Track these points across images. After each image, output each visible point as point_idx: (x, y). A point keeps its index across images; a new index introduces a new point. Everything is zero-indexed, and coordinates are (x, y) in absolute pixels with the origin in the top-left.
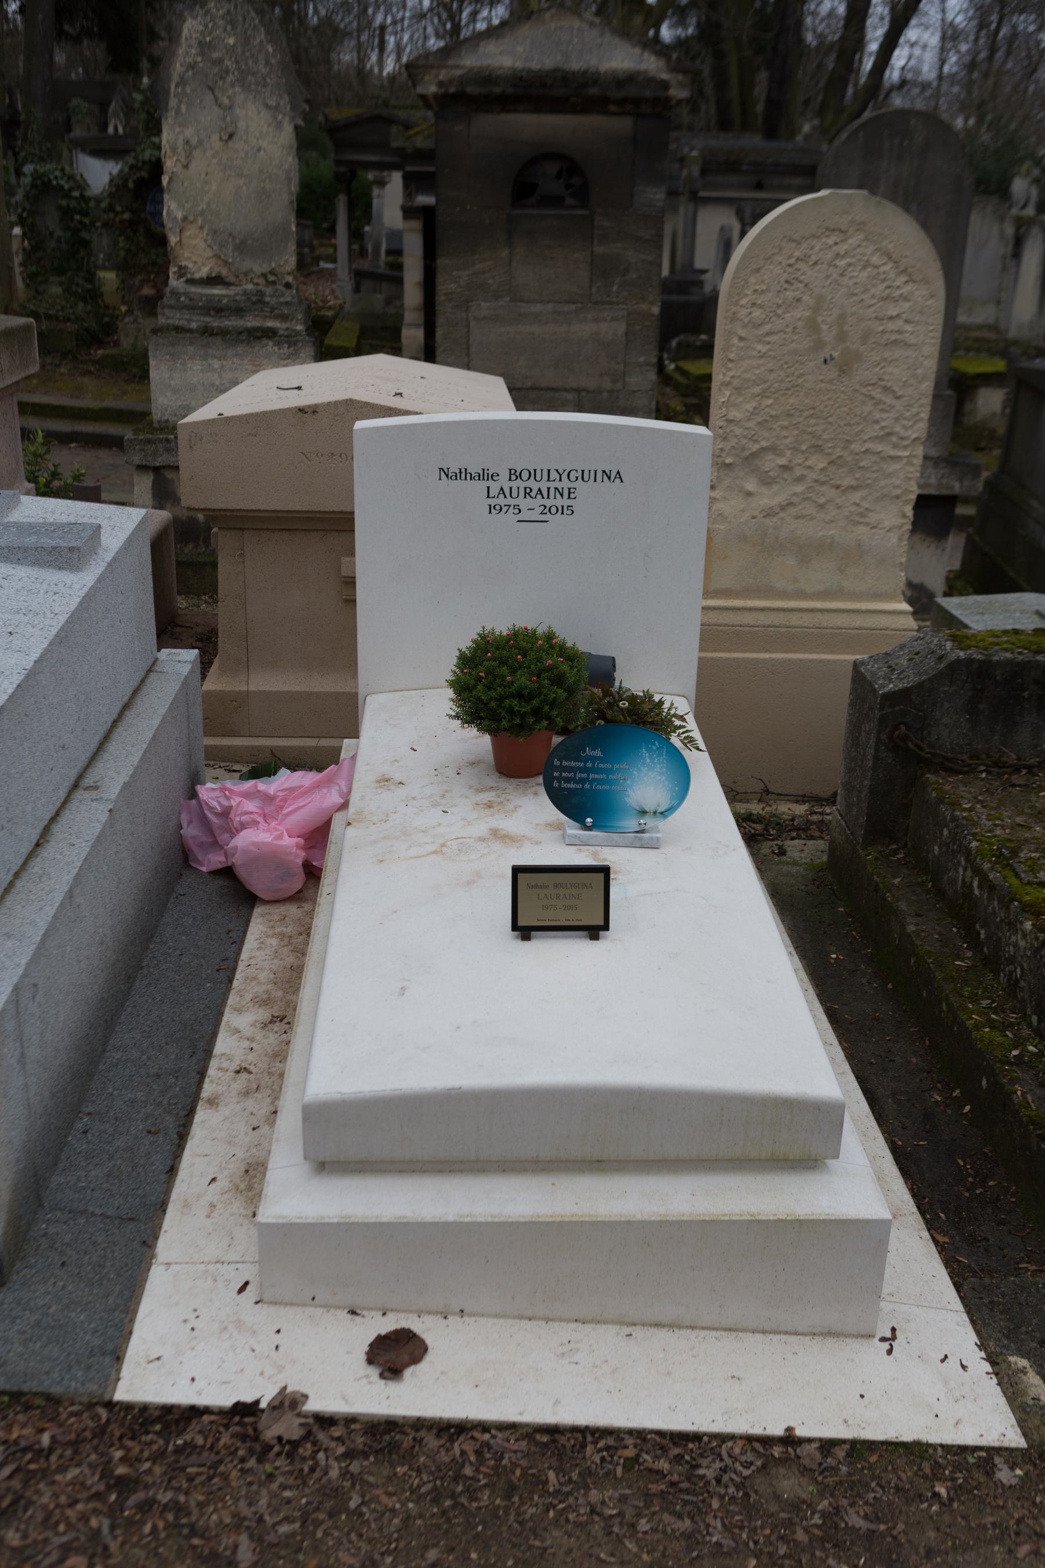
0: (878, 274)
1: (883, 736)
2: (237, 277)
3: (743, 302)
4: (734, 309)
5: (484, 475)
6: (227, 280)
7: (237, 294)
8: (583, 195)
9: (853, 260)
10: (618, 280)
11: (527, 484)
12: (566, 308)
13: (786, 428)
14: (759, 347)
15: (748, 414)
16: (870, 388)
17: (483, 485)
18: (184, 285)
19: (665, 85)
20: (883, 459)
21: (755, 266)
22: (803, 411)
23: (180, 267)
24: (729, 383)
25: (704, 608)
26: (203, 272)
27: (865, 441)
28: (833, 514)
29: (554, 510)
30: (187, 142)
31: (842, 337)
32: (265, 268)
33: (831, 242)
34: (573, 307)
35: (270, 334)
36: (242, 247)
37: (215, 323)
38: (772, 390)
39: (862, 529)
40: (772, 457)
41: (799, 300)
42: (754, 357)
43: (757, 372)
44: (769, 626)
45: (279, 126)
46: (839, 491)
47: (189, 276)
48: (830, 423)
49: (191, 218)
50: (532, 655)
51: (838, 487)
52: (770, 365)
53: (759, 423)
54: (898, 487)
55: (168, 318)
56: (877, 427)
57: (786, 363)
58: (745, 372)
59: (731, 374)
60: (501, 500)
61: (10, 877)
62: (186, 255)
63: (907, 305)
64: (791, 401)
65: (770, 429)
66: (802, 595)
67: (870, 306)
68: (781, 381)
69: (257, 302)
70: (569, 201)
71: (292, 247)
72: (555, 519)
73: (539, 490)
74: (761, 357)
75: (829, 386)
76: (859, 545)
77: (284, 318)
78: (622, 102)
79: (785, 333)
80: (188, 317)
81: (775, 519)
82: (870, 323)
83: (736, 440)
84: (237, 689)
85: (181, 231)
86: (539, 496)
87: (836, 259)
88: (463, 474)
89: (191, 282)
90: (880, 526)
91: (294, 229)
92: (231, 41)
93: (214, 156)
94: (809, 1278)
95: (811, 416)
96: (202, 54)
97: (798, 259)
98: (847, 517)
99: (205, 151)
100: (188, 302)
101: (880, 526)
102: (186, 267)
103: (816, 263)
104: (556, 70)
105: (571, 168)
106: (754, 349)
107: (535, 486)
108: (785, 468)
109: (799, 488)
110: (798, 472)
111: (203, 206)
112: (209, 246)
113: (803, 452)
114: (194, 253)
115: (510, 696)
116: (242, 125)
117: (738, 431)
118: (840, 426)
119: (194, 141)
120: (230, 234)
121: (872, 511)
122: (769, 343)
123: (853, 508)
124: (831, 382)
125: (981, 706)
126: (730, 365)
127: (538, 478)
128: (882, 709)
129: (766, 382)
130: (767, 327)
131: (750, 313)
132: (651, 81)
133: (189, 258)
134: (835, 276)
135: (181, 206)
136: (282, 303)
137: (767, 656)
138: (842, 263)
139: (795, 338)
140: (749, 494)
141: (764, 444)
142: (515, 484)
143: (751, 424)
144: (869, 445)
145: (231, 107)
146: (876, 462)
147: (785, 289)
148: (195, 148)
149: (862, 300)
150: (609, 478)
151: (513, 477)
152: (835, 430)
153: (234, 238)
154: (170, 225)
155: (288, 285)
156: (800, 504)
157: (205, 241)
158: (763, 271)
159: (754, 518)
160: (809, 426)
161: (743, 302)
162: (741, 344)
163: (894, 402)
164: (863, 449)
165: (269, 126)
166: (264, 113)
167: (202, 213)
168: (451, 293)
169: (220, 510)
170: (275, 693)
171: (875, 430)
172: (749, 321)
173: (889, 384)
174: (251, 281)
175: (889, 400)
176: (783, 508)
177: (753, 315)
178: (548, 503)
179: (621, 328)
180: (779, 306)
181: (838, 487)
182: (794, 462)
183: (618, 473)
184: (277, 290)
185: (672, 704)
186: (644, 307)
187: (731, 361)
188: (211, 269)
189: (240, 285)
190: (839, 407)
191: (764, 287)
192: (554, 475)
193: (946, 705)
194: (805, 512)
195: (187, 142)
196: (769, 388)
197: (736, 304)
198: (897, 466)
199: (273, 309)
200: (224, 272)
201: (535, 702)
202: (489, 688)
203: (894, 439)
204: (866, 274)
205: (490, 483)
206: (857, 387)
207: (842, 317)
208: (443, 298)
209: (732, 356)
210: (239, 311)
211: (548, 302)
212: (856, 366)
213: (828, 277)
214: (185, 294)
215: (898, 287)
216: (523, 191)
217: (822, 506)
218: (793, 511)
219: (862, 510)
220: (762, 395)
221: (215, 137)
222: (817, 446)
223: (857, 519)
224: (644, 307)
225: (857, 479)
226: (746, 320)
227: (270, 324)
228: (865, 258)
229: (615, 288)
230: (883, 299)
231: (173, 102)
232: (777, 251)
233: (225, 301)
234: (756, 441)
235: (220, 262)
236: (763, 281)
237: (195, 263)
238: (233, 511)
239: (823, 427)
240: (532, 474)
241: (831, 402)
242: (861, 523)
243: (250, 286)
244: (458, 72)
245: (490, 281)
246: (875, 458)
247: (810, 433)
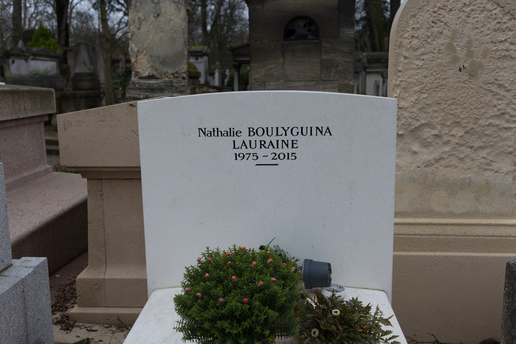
0: (491, 15)
2: (161, 75)
3: (406, 35)
4: (400, 40)
6: (157, 77)
7: (161, 83)
8: (316, 34)
9: (474, 8)
10: (334, 70)
11: (262, 138)
13: (437, 111)
14: (417, 62)
15: (412, 103)
16: (490, 85)
17: (231, 139)
18: (138, 80)
20: (500, 129)
21: (412, 14)
22: (447, 101)
23: (136, 72)
24: (399, 85)
25: (396, 224)
26: (146, 74)
27: (488, 118)
28: (469, 164)
29: (282, 156)
30: (139, 19)
31: (470, 54)
32: (173, 71)
34: (313, 83)
36: (163, 62)
38: (427, 88)
39: (488, 174)
40: (428, 130)
41: (441, 33)
42: (415, 69)
43: (417, 78)
44: (432, 235)
46: (472, 149)
47: (140, 76)
48: (465, 108)
49: (141, 51)
50: (246, 275)
51: (471, 148)
52: (424, 73)
53: (419, 109)
54: (511, 146)
55: (130, 94)
56: (495, 109)
57: (435, 71)
58: (409, 78)
59: (400, 79)
60: (244, 150)
62: (139, 67)
63: (511, 33)
64: (439, 95)
65: (426, 112)
66: (452, 215)
67: (487, 35)
68: (432, 83)
70: (310, 37)
72: (283, 163)
73: (271, 142)
74: (419, 68)
75: (463, 85)
76: (488, 183)
79: (433, 53)
80: (138, 93)
81: (432, 168)
82: (487, 45)
83: (405, 120)
84: (98, 277)
85: (136, 56)
86: (271, 147)
87: (463, 7)
88: (216, 132)
89: (141, 78)
90: (501, 171)
91: (186, 53)
93: (151, 24)
95: (452, 104)
97: (439, 8)
98: (479, 166)
99: (147, 22)
100: (139, 86)
101: (501, 171)
102: (139, 72)
103: (451, 10)
106: (414, 64)
107: (267, 139)
108: (437, 136)
109: (447, 149)
110: (445, 138)
111: (146, 45)
112: (149, 62)
113: (448, 126)
115: (222, 318)
116: (163, 10)
117: (406, 114)
118: (471, 109)
119: (143, 18)
120: (158, 57)
121: (494, 162)
122: (423, 60)
123: (482, 160)
124: (464, 82)
126: (399, 74)
127: (270, 134)
129: (422, 83)
130: (422, 50)
131: (411, 42)
133: (140, 68)
134: (464, 17)
135: (137, 46)
136: (181, 86)
137: (432, 254)
138: (468, 9)
139: (440, 56)
140: (415, 153)
141: (423, 122)
142: (253, 138)
143: (414, 110)
144: (490, 121)
145: (158, 3)
146: (496, 131)
147: (432, 27)
148: (143, 21)
149: (482, 31)
150: (321, 132)
151: (252, 134)
152: (468, 112)
153: (160, 58)
154: (132, 54)
155: (184, 78)
156: (447, 158)
157: (147, 60)
158: (417, 16)
159: (418, 167)
160: (451, 110)
161: (406, 35)
162: (406, 61)
163: (506, 94)
164: (487, 123)
165: (175, 10)
166: (173, 5)
167: (146, 48)
168: (257, 79)
169: (84, 167)
170: (121, 280)
171: (494, 112)
172: (410, 47)
173: (502, 83)
174: (167, 77)
175: (502, 92)
176: (437, 161)
177: (412, 43)
178: (278, 151)
180: (429, 37)
181: (471, 148)
182: (443, 132)
183: (328, 128)
184: (179, 80)
185: (378, 309)
186: (346, 82)
187: (400, 71)
188: (150, 72)
189: (162, 79)
190: (471, 97)
191: (419, 26)
194: (451, 163)
195: (139, 19)
196: (424, 87)
197: (401, 37)
198: (509, 134)
199: (176, 88)
200: (155, 73)
201: (246, 324)
202: (205, 307)
203: (507, 117)
204: (483, 16)
205: (235, 138)
206: (482, 85)
207: (469, 42)
208: (253, 81)
209: (400, 68)
211: (301, 81)
212: (480, 72)
213: (459, 18)
214: (138, 83)
215: (505, 23)
216: (289, 33)
217: (462, 160)
218: (443, 162)
219: (488, 161)
220: (421, 92)
221: (152, 16)
222: (457, 122)
223: (485, 167)
224: (346, 82)
225: (483, 142)
226: (408, 46)
228: (483, 6)
229: (332, 74)
230: (495, 30)
232: (426, 3)
233: (156, 86)
234: (418, 120)
235: (153, 69)
236: (418, 22)
237: (143, 70)
238: (93, 167)
239: (460, 110)
240: (265, 131)
241: (465, 95)
242: (488, 169)
243: (167, 79)
245: (275, 73)
246: (495, 129)
247: (452, 114)
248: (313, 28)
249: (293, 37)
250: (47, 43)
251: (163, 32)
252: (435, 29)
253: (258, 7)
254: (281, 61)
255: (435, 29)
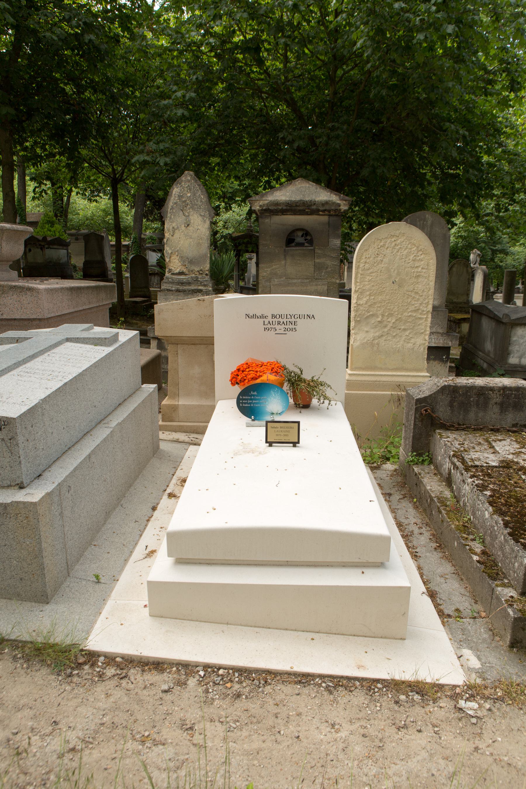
1: (417, 416)
5: (262, 317)
8: (311, 242)
12: (306, 281)
14: (368, 278)
17: (262, 320)
19: (339, 205)
20: (416, 319)
26: (177, 271)
30: (173, 228)
31: (399, 274)
33: (393, 240)
35: (200, 291)
36: (191, 262)
37: (181, 288)
45: (205, 222)
60: (269, 326)
61: (66, 449)
69: (196, 280)
70: (306, 244)
71: (208, 261)
77: (205, 286)
78: (324, 211)
88: (254, 316)
89: (173, 274)
92: (189, 195)
94: (385, 620)
96: (179, 199)
104: (301, 200)
105: (306, 233)
107: (282, 321)
114: (174, 264)
116: (192, 221)
117: (361, 308)
125: (455, 404)
128: (416, 404)
132: (333, 203)
142: (274, 320)
155: (207, 275)
166: (200, 218)
167: (178, 251)
171: (412, 308)
178: (287, 327)
179: (326, 288)
186: (334, 280)
192: (289, 316)
193: (441, 403)
195: (173, 228)
200: (185, 270)
205: (265, 319)
210: (189, 284)
216: (290, 241)
218: (384, 338)
224: (334, 280)
227: (200, 288)
231: (169, 215)
244: (267, 202)
248: (309, 238)
249: (293, 244)
250: (52, 229)
251: (191, 238)
252: (379, 259)
253: (267, 221)
254: (283, 262)
255: (379, 259)
